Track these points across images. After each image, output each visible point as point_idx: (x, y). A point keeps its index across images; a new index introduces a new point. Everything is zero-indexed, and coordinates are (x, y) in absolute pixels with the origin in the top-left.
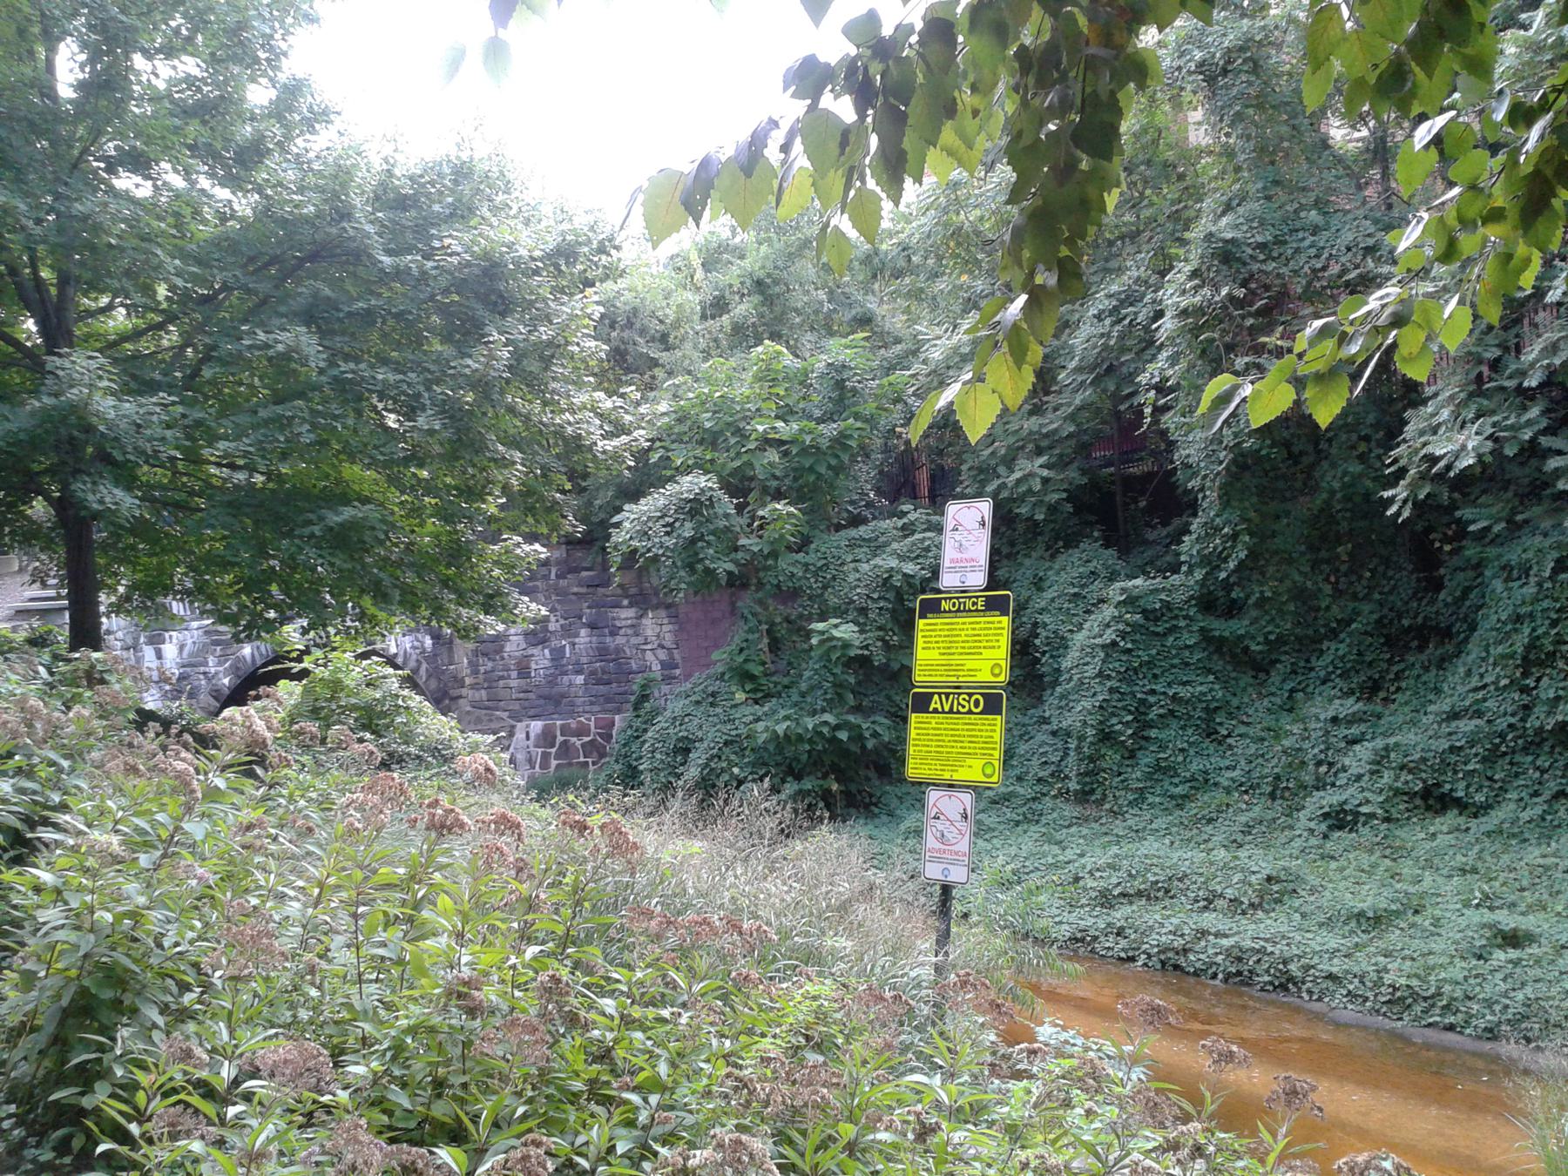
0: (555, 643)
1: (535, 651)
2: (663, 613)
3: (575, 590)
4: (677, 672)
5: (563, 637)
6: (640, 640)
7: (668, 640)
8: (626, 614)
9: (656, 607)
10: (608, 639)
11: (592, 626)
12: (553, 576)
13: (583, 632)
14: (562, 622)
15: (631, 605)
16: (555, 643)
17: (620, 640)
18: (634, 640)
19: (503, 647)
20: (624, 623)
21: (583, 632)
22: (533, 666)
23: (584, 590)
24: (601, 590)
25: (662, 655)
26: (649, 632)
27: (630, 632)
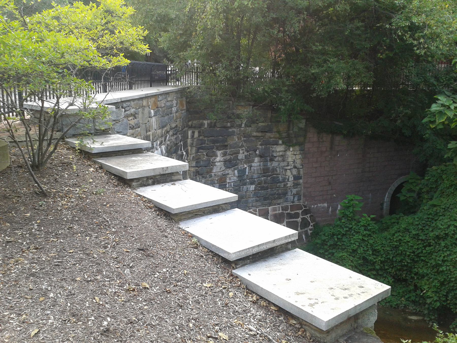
0: (240, 166)
1: (230, 171)
2: (297, 148)
3: (255, 134)
4: (301, 181)
5: (245, 163)
6: (285, 164)
7: (298, 162)
8: (280, 149)
9: (293, 146)
10: (269, 164)
11: (261, 156)
12: (243, 125)
13: (256, 159)
14: (246, 153)
15: (283, 143)
16: (240, 166)
17: (275, 164)
18: (282, 164)
19: (212, 169)
20: (278, 154)
21: (256, 159)
22: (228, 181)
23: (259, 134)
24: (268, 134)
25: (295, 172)
26: (290, 159)
27: (280, 159)
